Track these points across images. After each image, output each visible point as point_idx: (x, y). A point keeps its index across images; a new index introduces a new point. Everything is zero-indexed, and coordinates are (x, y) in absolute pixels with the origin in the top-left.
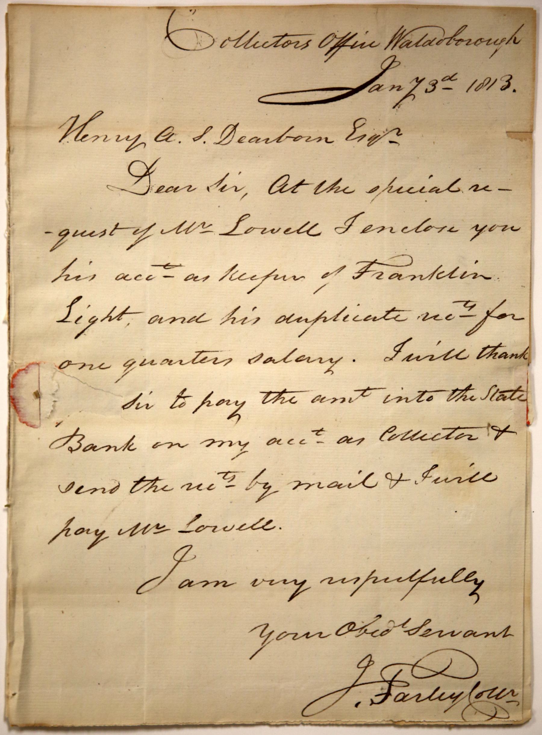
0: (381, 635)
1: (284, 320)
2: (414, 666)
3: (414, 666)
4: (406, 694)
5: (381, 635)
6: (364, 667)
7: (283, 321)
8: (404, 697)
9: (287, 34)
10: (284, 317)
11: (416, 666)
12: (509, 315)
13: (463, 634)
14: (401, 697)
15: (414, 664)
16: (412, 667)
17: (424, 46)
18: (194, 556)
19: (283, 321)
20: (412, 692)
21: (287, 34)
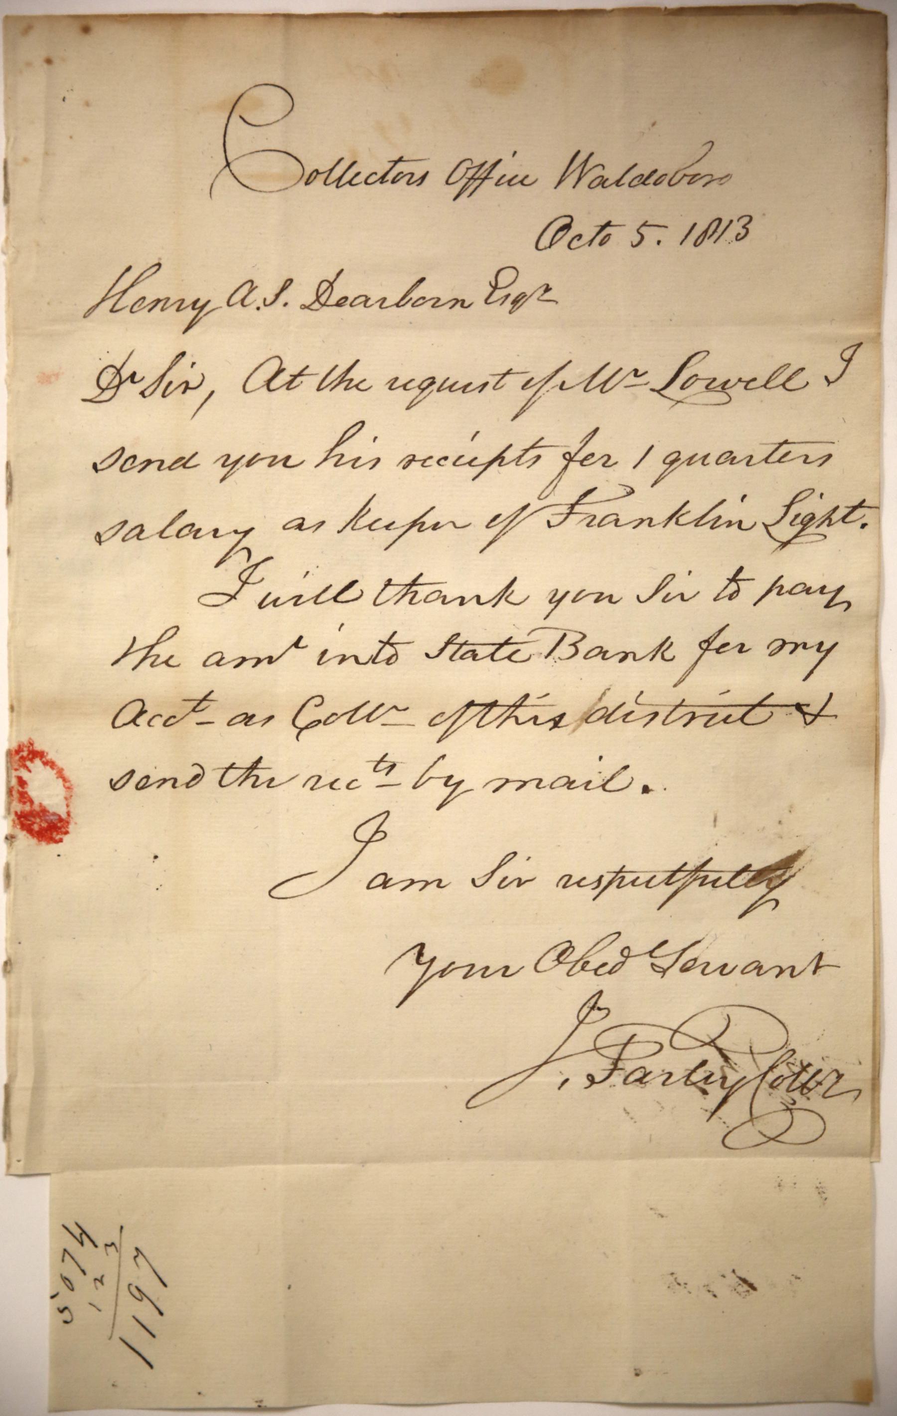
0: (610, 972)
1: (599, 653)
2: (676, 1031)
3: (676, 1031)
4: (648, 1071)
5: (610, 972)
6: (621, 1044)
7: (596, 656)
8: (645, 1075)
9: (787, 440)
10: (438, 593)
11: (680, 1032)
12: (837, 522)
13: (738, 970)
14: (639, 1075)
15: (675, 1028)
16: (671, 1032)
17: (455, 299)
18: (151, 724)
19: (596, 656)
20: (655, 1065)
21: (787, 440)
